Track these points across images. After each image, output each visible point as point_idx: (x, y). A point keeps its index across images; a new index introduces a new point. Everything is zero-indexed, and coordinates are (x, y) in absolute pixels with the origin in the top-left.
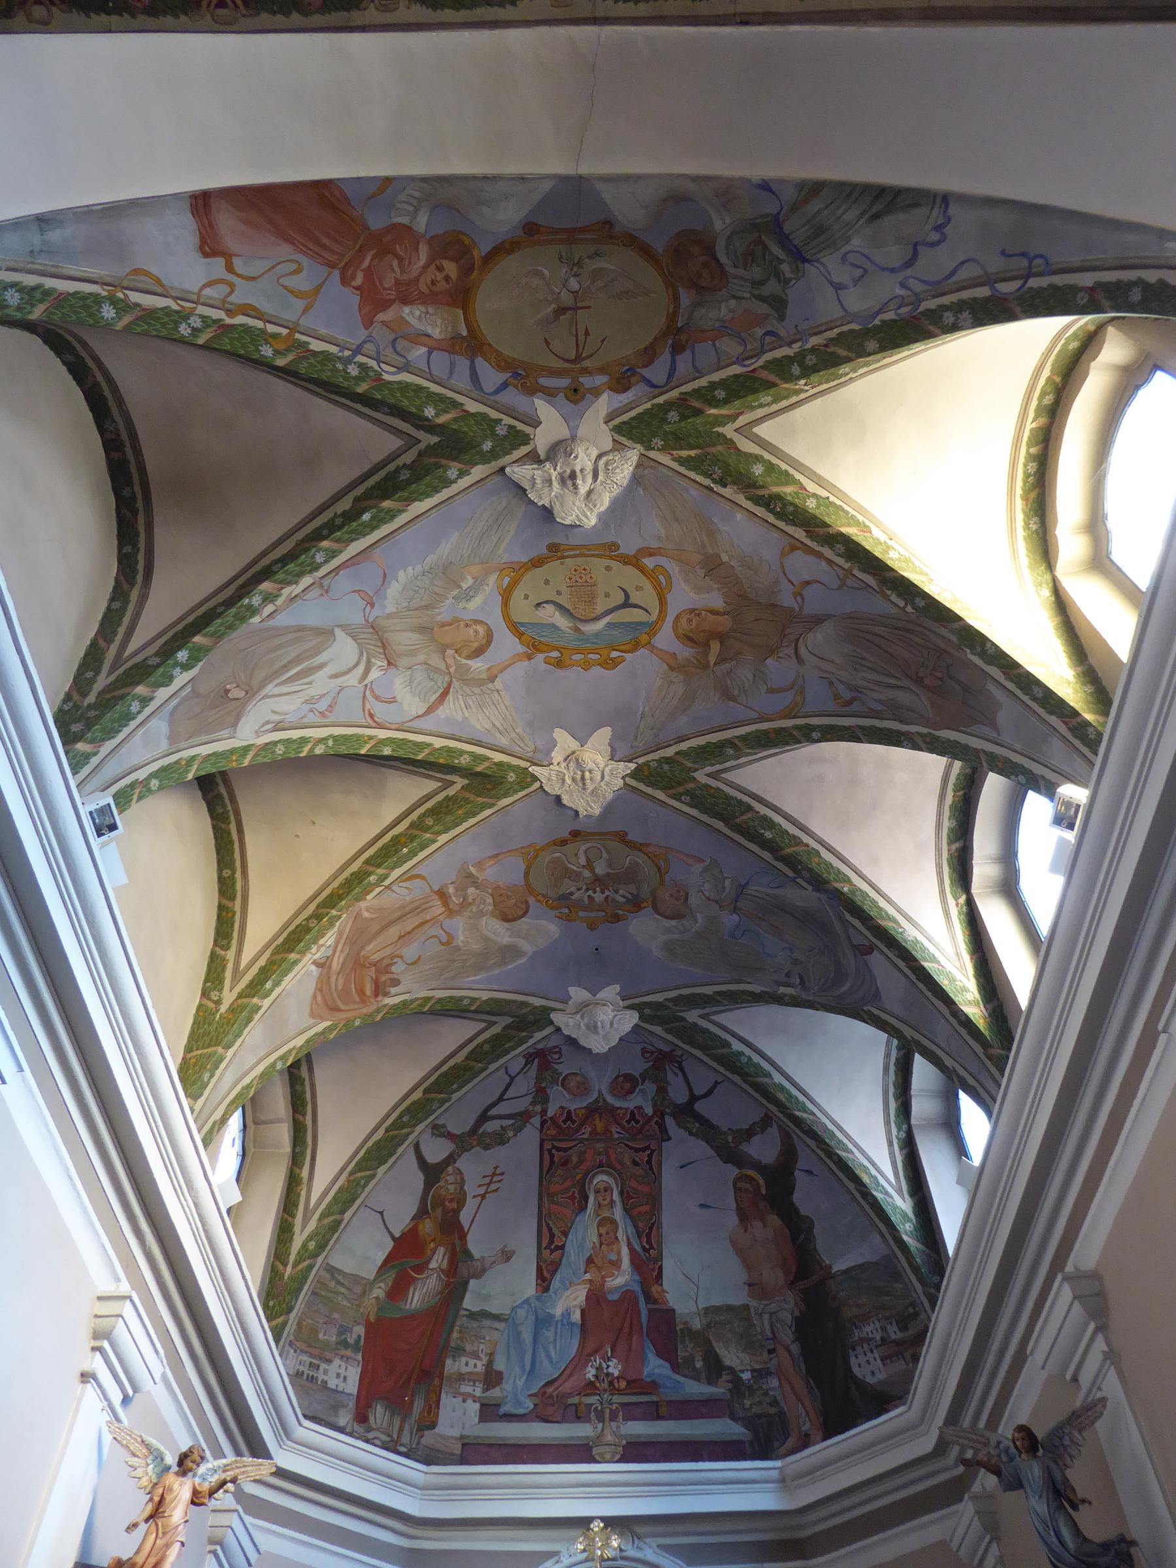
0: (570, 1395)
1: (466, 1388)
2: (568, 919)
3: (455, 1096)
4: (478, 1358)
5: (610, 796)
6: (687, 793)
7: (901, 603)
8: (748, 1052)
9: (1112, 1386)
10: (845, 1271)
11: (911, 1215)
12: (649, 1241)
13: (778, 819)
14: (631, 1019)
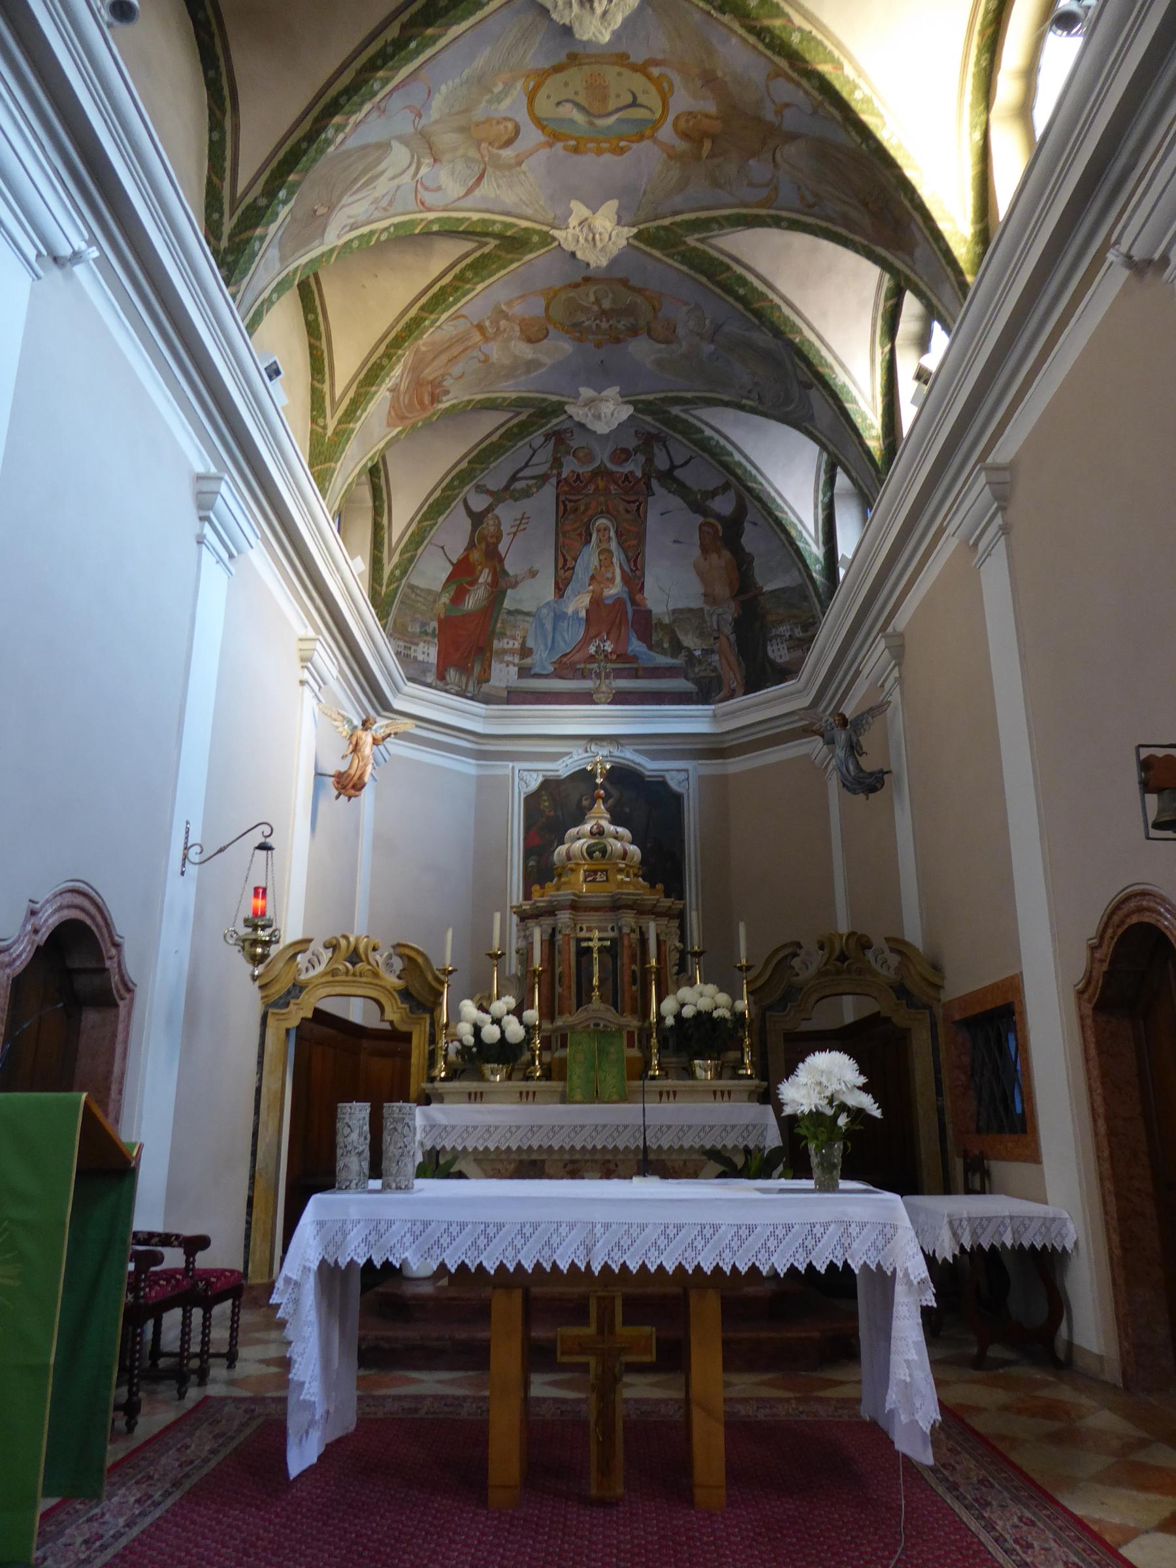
0: (579, 663)
1: (508, 658)
2: (580, 340)
3: (492, 466)
4: (514, 639)
5: (615, 252)
6: (678, 253)
7: (859, 140)
8: (716, 436)
9: (896, 697)
10: (771, 592)
11: (821, 559)
12: (635, 565)
13: (750, 278)
14: (626, 412)
